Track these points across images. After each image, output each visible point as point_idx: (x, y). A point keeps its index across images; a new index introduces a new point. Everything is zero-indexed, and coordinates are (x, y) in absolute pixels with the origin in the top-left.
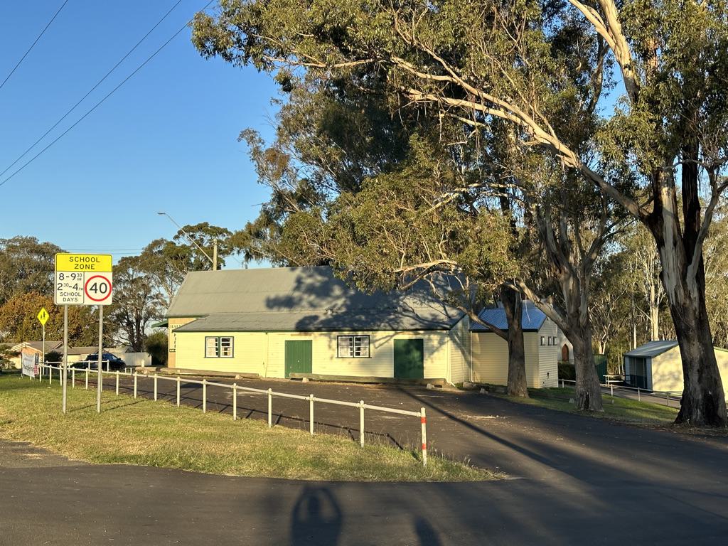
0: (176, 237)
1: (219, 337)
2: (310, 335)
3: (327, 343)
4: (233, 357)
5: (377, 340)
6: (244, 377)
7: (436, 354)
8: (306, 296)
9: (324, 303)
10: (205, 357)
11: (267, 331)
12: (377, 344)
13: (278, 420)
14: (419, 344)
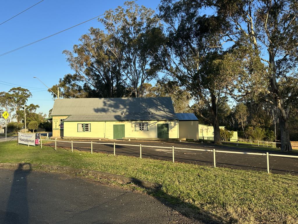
0: (10, 91)
1: (84, 124)
2: (124, 123)
3: (131, 125)
4: (90, 132)
5: (151, 124)
6: (102, 140)
7: (173, 129)
8: (110, 108)
9: (118, 111)
10: (78, 132)
11: (105, 121)
12: (150, 125)
13: (118, 153)
14: (167, 126)
